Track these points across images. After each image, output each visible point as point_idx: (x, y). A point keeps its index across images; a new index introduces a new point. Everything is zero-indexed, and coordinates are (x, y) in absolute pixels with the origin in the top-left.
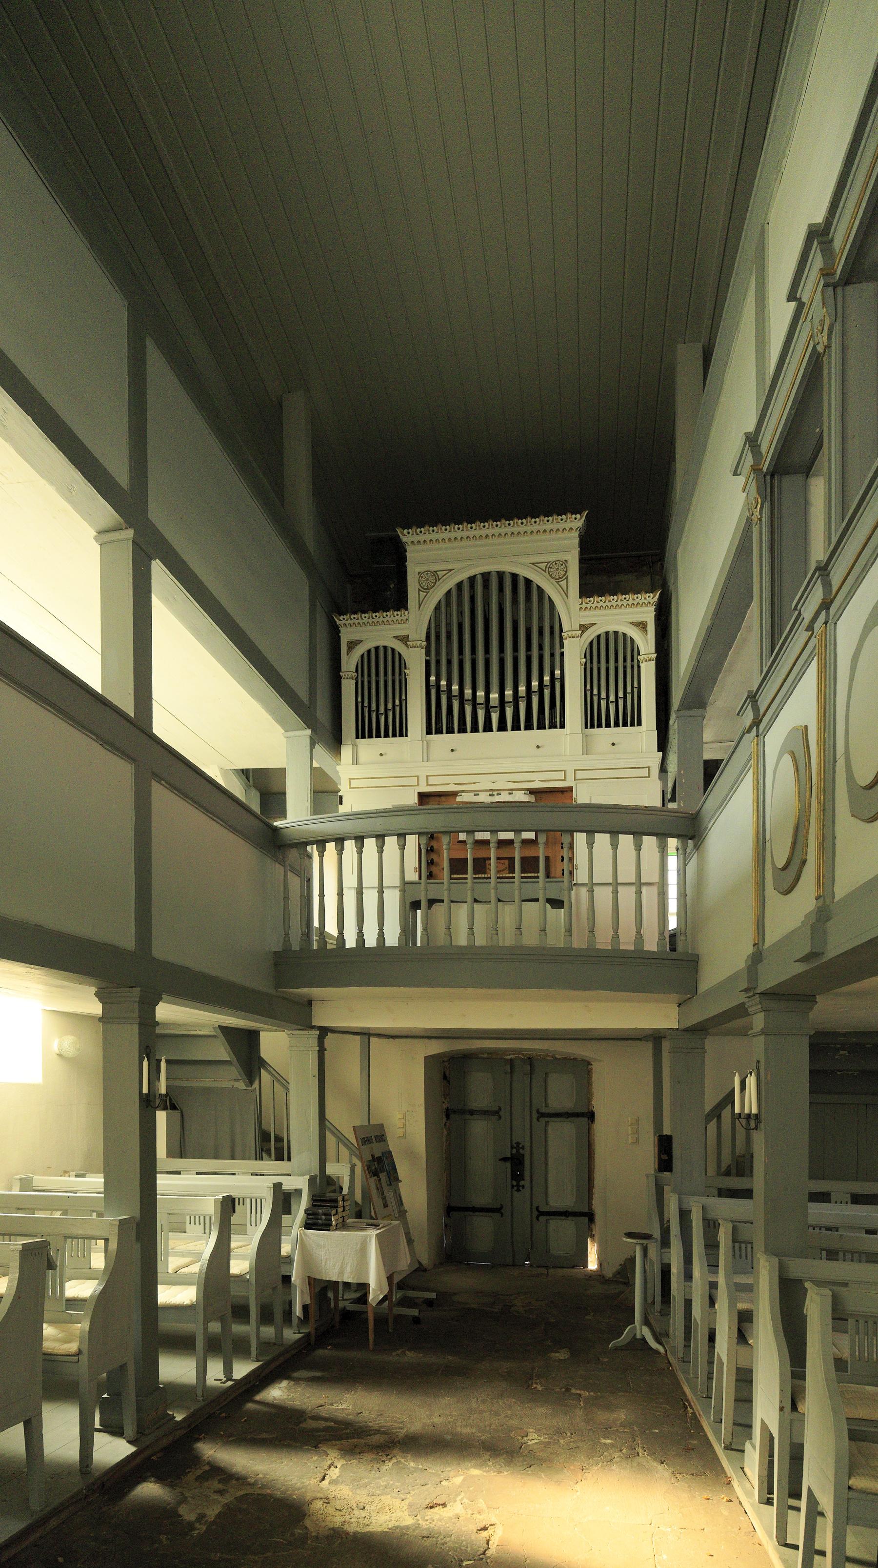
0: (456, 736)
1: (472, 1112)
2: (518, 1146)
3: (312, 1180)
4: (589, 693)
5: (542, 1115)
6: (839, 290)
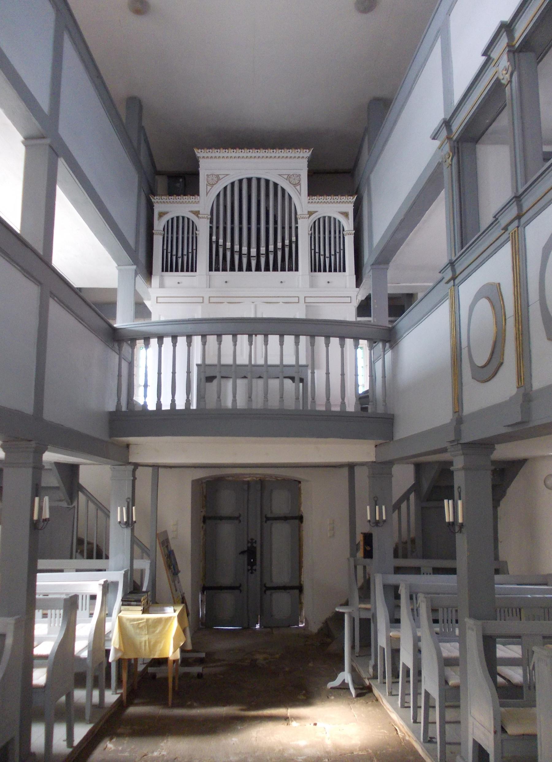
0: (229, 273)
1: (221, 518)
2: (252, 541)
3: (125, 575)
4: (313, 251)
5: (268, 519)
6: (516, 54)
